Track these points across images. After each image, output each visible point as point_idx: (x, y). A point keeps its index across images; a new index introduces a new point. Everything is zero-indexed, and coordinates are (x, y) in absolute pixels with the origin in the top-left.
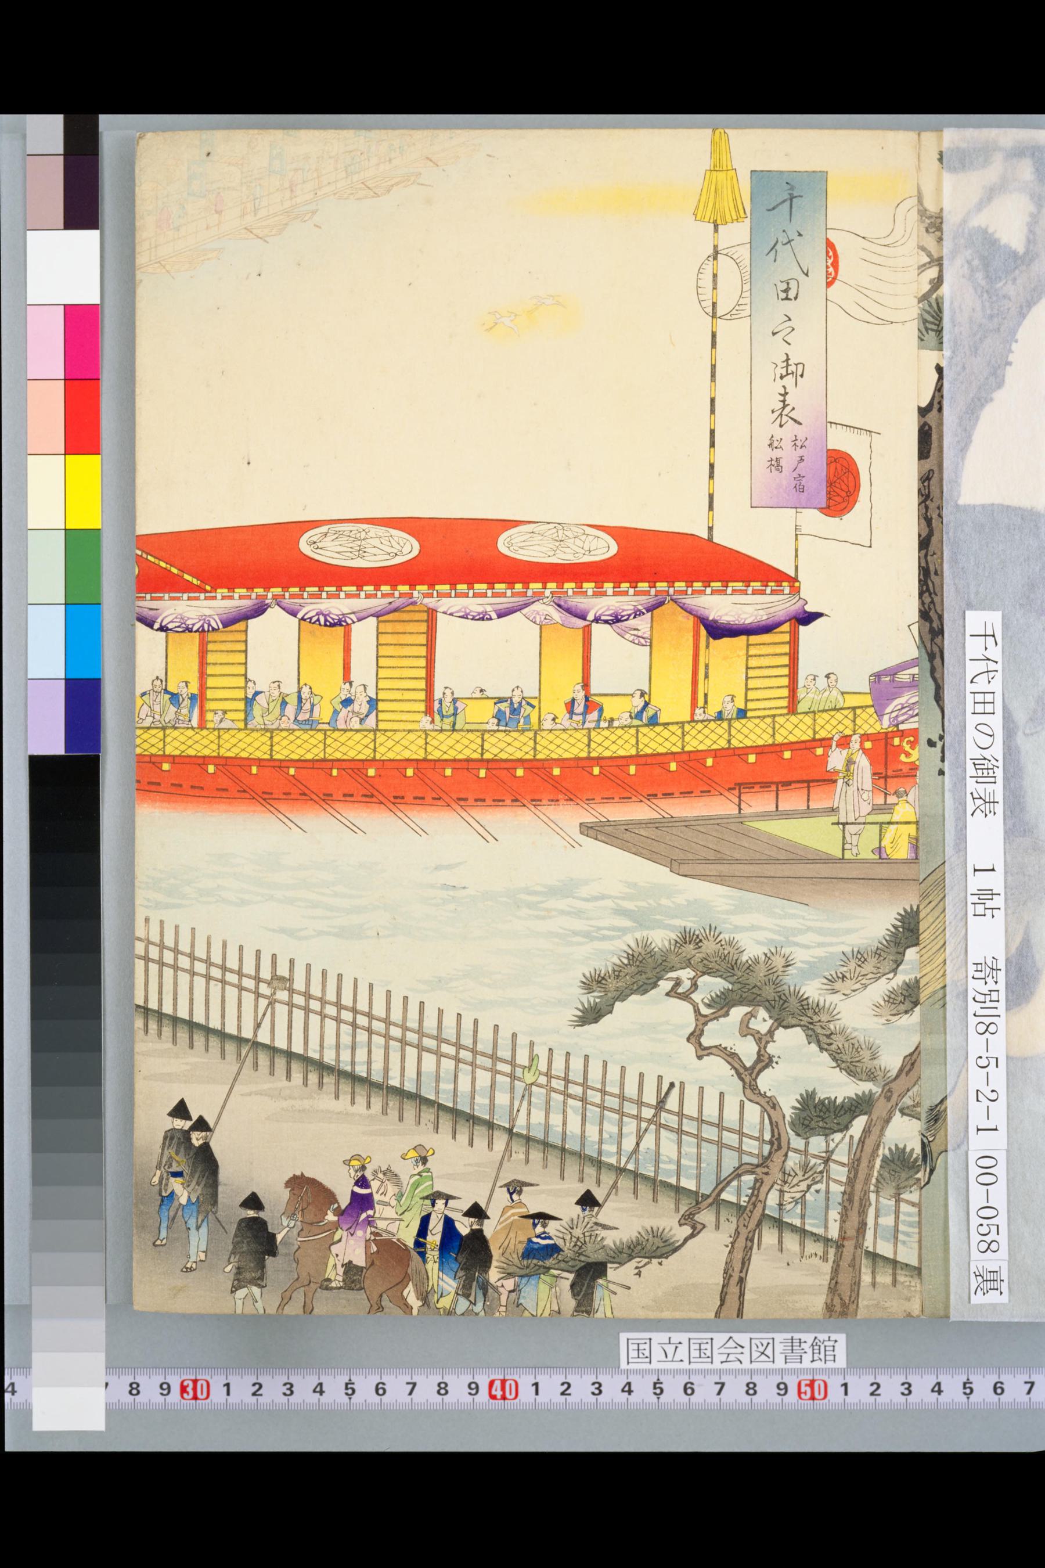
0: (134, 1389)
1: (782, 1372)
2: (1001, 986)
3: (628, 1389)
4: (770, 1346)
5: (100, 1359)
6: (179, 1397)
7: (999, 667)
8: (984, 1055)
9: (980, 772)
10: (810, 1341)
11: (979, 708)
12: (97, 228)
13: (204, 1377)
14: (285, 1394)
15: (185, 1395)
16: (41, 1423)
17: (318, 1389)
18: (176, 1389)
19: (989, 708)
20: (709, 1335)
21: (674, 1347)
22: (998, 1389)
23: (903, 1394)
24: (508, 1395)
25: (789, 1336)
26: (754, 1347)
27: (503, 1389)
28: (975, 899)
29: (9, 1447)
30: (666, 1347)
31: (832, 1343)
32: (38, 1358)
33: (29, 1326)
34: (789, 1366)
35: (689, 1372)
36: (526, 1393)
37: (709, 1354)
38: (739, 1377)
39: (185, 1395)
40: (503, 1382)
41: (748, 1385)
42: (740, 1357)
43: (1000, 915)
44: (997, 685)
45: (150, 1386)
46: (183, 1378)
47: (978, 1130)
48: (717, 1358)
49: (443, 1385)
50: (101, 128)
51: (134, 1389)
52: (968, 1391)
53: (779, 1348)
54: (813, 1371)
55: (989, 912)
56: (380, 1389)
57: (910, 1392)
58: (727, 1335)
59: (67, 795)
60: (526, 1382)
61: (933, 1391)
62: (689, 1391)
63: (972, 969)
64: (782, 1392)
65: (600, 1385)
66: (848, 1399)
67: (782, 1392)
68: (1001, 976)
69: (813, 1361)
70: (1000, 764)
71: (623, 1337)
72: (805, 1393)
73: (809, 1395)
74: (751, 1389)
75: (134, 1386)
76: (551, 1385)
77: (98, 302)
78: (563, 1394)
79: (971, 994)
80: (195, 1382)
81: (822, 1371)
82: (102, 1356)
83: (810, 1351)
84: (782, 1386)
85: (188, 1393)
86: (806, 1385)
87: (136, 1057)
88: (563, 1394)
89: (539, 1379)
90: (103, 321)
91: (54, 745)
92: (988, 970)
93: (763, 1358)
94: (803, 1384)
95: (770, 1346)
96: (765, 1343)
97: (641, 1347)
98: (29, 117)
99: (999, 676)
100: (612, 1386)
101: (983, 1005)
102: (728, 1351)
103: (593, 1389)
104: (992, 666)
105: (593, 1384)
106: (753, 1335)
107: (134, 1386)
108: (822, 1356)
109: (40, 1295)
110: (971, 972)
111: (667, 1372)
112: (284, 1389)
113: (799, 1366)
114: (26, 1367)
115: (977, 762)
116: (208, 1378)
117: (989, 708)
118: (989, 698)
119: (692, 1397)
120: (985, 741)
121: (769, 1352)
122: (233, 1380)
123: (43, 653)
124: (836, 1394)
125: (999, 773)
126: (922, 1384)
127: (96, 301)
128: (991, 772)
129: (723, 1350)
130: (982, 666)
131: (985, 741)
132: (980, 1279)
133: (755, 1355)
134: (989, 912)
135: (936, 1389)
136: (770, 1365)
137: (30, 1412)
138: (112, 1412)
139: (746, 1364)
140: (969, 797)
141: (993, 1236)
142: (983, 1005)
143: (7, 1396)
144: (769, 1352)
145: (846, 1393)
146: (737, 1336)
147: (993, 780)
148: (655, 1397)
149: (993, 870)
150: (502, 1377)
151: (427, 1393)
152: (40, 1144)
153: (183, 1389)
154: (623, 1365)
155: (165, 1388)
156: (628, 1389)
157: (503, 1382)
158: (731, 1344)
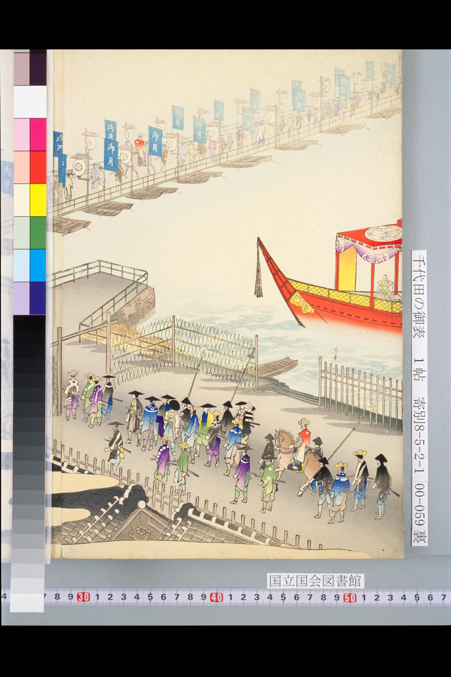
0: (57, 596)
1: (337, 590)
2: (426, 410)
3: (270, 597)
4: (332, 579)
5: (41, 582)
6: (77, 600)
7: (426, 274)
8: (418, 439)
9: (417, 319)
10: (349, 577)
15: (79, 599)
16: (12, 610)
18: (75, 597)
19: (421, 292)
20: (306, 574)
22: (430, 598)
23: (122, 599)
25: (340, 575)
26: (325, 580)
27: (216, 597)
28: (415, 373)
30: (287, 579)
31: (358, 578)
32: (13, 581)
34: (340, 587)
35: (297, 590)
36: (226, 599)
37: (305, 582)
39: (79, 599)
40: (217, 594)
42: (319, 584)
43: (426, 380)
44: (425, 282)
46: (78, 592)
48: (309, 584)
49: (57, 595)
51: (57, 596)
52: (283, 598)
53: (336, 580)
55: (421, 378)
58: (313, 574)
59: (30, 331)
60: (226, 594)
61: (402, 598)
62: (297, 598)
63: (413, 402)
64: (337, 599)
66: (365, 602)
67: (337, 599)
68: (426, 406)
69: (350, 585)
70: (426, 315)
71: (268, 575)
72: (347, 599)
73: (348, 600)
74: (323, 597)
75: (190, 596)
76: (237, 595)
78: (242, 599)
80: (83, 593)
81: (354, 590)
82: (43, 580)
83: (349, 581)
85: (80, 598)
86: (347, 596)
88: (242, 599)
89: (232, 593)
91: (26, 311)
92: (420, 403)
93: (329, 584)
95: (332, 579)
96: (329, 578)
99: (426, 278)
100: (264, 596)
101: (418, 418)
103: (255, 597)
104: (423, 274)
105: (255, 595)
106: (324, 574)
107: (190, 596)
108: (354, 583)
112: (122, 597)
113: (344, 587)
114: (9, 587)
115: (416, 314)
116: (89, 592)
117: (421, 292)
118: (421, 287)
119: (298, 601)
120: (420, 306)
121: (331, 581)
122: (100, 593)
123: (18, 269)
124: (360, 600)
125: (426, 319)
126: (397, 596)
128: (422, 319)
129: (311, 581)
130: (418, 274)
131: (420, 306)
133: (325, 583)
134: (421, 379)
136: (332, 587)
138: (46, 606)
139: (321, 587)
140: (413, 329)
141: (422, 518)
142: (418, 418)
143: (3, 599)
144: (331, 581)
145: (98, 599)
147: (423, 322)
148: (149, 600)
149: (423, 360)
151: (183, 598)
153: (78, 597)
154: (268, 587)
155: (71, 596)
156: (270, 597)
157: (217, 594)
158: (315, 578)
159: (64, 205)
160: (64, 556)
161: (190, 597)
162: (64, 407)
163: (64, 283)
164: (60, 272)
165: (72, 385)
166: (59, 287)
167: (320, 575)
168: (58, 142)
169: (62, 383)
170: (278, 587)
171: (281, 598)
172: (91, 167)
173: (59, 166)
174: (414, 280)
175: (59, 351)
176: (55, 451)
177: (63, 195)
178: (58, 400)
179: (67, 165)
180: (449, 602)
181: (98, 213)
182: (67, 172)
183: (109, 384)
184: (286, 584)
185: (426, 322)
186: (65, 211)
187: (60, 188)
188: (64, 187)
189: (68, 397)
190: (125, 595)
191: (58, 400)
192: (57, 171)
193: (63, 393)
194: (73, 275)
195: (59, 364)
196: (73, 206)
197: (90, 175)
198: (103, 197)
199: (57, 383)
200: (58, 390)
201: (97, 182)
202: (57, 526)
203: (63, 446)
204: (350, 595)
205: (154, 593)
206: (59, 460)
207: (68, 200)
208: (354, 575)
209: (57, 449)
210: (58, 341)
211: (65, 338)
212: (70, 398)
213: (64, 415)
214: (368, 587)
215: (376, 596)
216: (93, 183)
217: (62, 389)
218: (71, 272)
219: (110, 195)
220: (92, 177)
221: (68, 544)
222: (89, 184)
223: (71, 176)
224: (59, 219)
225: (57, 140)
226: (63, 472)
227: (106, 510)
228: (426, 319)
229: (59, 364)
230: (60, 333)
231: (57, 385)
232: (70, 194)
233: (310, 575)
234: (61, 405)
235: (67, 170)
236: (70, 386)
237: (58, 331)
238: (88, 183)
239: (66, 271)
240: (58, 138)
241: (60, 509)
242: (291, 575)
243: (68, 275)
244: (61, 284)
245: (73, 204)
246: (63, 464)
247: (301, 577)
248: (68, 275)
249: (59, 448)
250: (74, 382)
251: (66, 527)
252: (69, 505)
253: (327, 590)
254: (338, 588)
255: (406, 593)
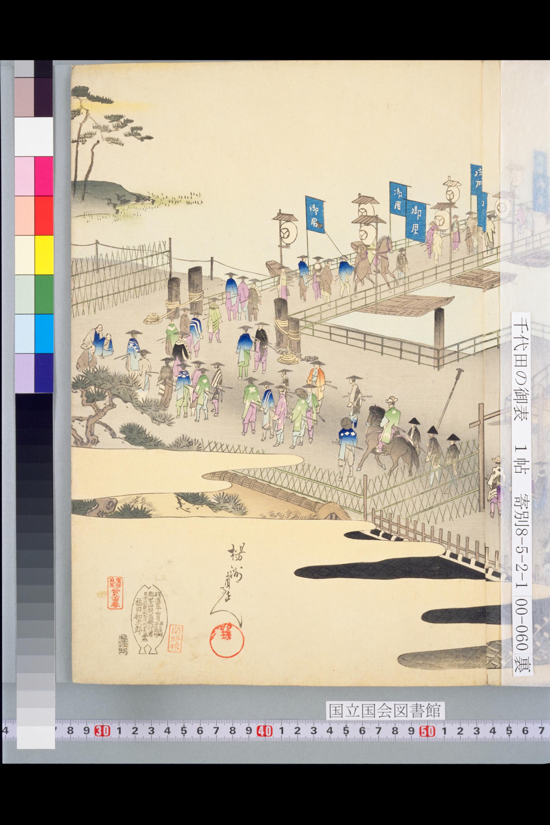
0: (70, 730)
1: (411, 722)
2: (530, 510)
3: (330, 731)
4: (405, 708)
5: (51, 712)
8: (520, 546)
9: (519, 397)
11: (519, 363)
12: (51, 234)
13: (107, 724)
14: (150, 733)
16: (20, 746)
17: (167, 731)
18: (92, 731)
19: (524, 363)
20: (373, 703)
21: (354, 709)
23: (475, 733)
24: (267, 734)
25: (415, 703)
26: (397, 709)
27: (265, 730)
28: (516, 464)
29: (4, 762)
30: (350, 709)
31: (438, 707)
32: (20, 712)
33: (15, 697)
34: (415, 719)
35: (363, 722)
37: (373, 712)
38: (389, 725)
39: (97, 734)
40: (265, 727)
41: (393, 729)
42: (389, 714)
44: (528, 351)
45: (79, 729)
46: (96, 725)
47: (517, 585)
48: (377, 715)
50: (53, 64)
51: (70, 730)
52: (346, 732)
53: (410, 709)
54: (428, 721)
55: (523, 471)
56: (200, 731)
57: (479, 733)
58: (383, 703)
59: (35, 413)
60: (276, 727)
62: (362, 732)
63: (514, 500)
65: (316, 729)
66: (284, 736)
68: (530, 504)
69: (428, 716)
70: (529, 393)
71: (328, 703)
72: (424, 733)
74: (395, 731)
75: (70, 729)
76: (290, 728)
77: (52, 155)
79: (514, 514)
80: (102, 727)
82: (53, 710)
83: (426, 711)
84: (411, 729)
85: (99, 733)
87: (72, 407)
88: (459, 734)
89: (284, 725)
90: (55, 165)
91: (29, 388)
92: (523, 501)
93: (401, 714)
94: (422, 728)
95: (405, 708)
96: (402, 706)
97: (337, 708)
98: (15, 61)
99: (529, 346)
100: (322, 729)
102: (383, 711)
104: (525, 341)
105: (312, 728)
108: (432, 714)
109: (21, 678)
110: (514, 502)
111: (351, 722)
113: (420, 719)
114: (13, 719)
115: (517, 392)
117: (524, 363)
118: (524, 358)
119: (527, 735)
120: (522, 381)
123: (22, 340)
124: (439, 733)
126: (485, 729)
127: (51, 154)
128: (524, 397)
129: (380, 711)
130: (520, 341)
131: (522, 381)
132: (518, 664)
133: (397, 713)
135: (493, 731)
136: (405, 719)
137: (16, 742)
138: (58, 742)
139: (393, 718)
143: (4, 734)
144: (404, 711)
146: (387, 703)
147: (525, 401)
148: (508, 735)
149: (525, 448)
150: (264, 725)
152: (21, 598)
153: (96, 731)
154: (328, 718)
155: (87, 730)
156: (330, 731)
157: (265, 727)
158: (385, 707)
159: (485, 255)
160: (490, 683)
161: (233, 730)
162: (488, 501)
163: (486, 349)
164: (481, 336)
165: (497, 473)
166: (480, 354)
167: (390, 704)
168: (477, 177)
169: (485, 471)
170: (340, 719)
171: (506, 732)
172: (517, 208)
173: (478, 207)
174: (515, 349)
175: (481, 433)
176: (477, 554)
177: (484, 241)
178: (479, 492)
179: (488, 206)
180: (548, 737)
181: (526, 264)
182: (488, 214)
183: (542, 472)
184: (349, 715)
185: (529, 401)
186: (485, 261)
187: (480, 234)
188: (485, 232)
189: (493, 488)
190: (479, 729)
191: (479, 492)
192: (476, 212)
193: (486, 483)
194: (496, 340)
195: (480, 448)
196: (496, 256)
197: (516, 217)
198: (531, 244)
199: (479, 472)
200: (479, 480)
201: (524, 226)
202: (481, 647)
203: (487, 549)
204: (427, 728)
205: (514, 727)
206: (482, 566)
207: (489, 249)
208: (433, 703)
209: (480, 552)
210: (479, 420)
211: (487, 417)
212: (495, 490)
213: (487, 511)
214: (449, 717)
215: (459, 729)
216: (520, 227)
217: (484, 479)
218: (495, 335)
219: (539, 242)
220: (518, 220)
221: (495, 668)
222: (515, 228)
223: (492, 219)
224: (479, 272)
225: (476, 175)
226: (488, 580)
227: (541, 625)
228: (529, 397)
229: (480, 448)
230: (481, 410)
231: (479, 474)
232: (491, 241)
233: (379, 704)
234: (484, 499)
235: (488, 211)
236: (495, 476)
237: (479, 409)
238: (513, 227)
239: (487, 334)
240: (477, 172)
241: (483, 625)
242: (356, 703)
243: (490, 340)
244: (482, 351)
245: (496, 252)
246: (487, 570)
247: (368, 706)
248: (490, 340)
249: (482, 551)
250: (499, 470)
251: (492, 647)
252: (495, 621)
253: (400, 722)
254: (412, 719)
255: (495, 726)
